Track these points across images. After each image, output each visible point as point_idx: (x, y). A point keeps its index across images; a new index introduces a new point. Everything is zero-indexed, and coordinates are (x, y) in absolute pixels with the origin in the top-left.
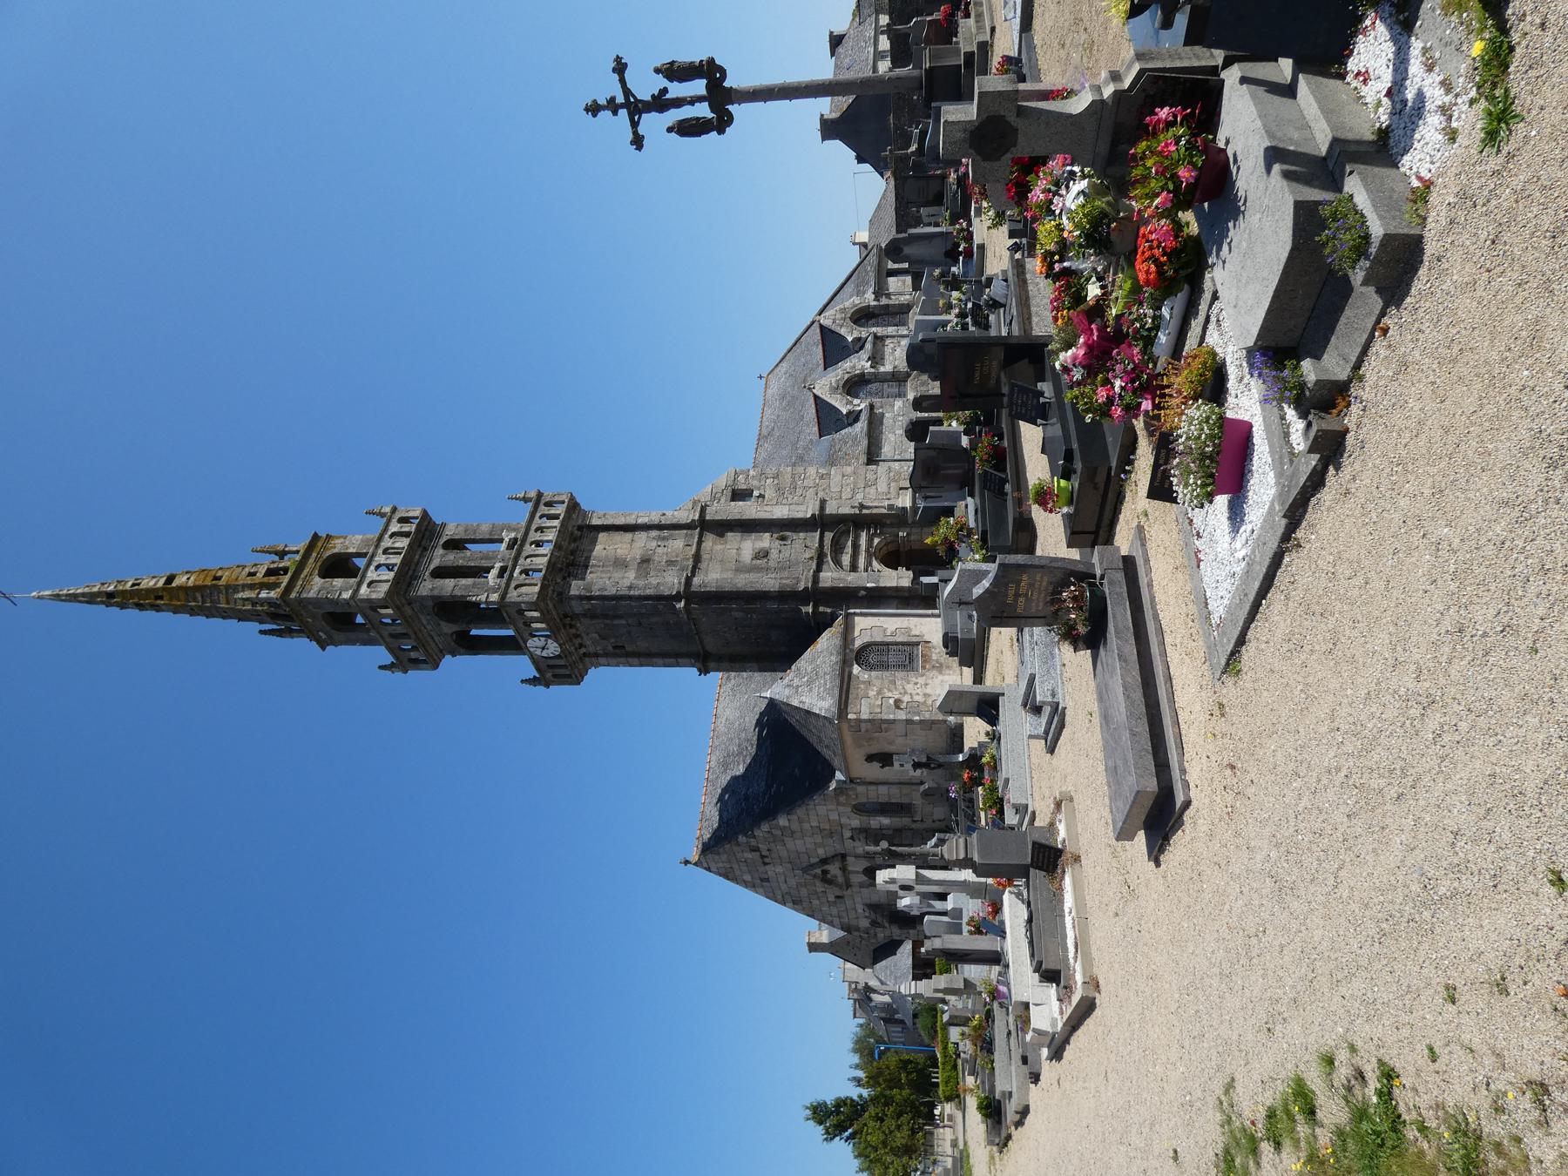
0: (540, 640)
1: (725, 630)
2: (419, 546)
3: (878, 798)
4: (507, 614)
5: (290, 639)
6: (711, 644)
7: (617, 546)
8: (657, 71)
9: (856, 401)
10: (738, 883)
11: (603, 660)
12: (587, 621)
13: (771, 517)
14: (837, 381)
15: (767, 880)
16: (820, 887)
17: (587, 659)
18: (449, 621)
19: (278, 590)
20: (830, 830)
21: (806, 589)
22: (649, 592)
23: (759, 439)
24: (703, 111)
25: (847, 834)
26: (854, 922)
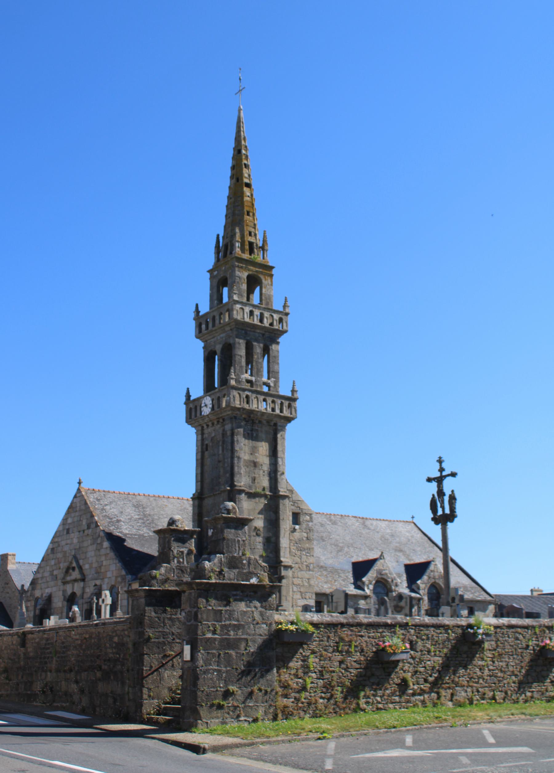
2: (266, 332)
5: (232, 155)
6: (208, 502)
7: (264, 447)
8: (453, 491)
9: (371, 587)
10: (66, 514)
11: (200, 437)
12: (221, 431)
14: (386, 574)
15: (68, 532)
16: (63, 565)
17: (200, 428)
19: (240, 253)
20: (101, 572)
22: (236, 469)
23: (363, 518)
24: (440, 512)
25: (98, 582)
26: (38, 587)
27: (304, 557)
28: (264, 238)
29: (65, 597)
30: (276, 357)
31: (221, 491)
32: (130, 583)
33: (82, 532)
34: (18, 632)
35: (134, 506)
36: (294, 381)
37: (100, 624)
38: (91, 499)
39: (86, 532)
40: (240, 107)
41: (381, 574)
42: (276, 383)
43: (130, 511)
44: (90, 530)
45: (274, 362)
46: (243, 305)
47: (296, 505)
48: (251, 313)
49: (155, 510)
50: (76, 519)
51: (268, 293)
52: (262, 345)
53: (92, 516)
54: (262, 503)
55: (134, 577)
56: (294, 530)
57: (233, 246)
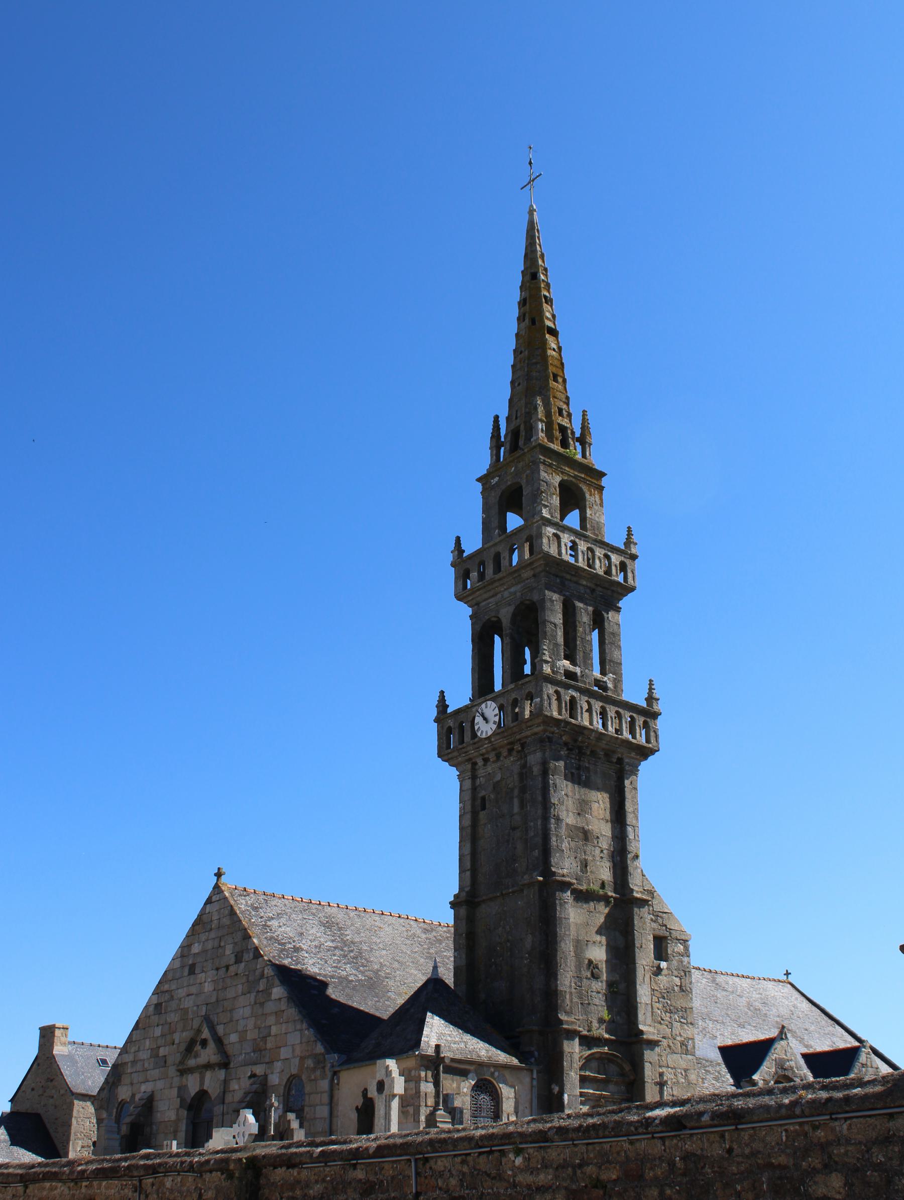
0: (495, 715)
1: (508, 927)
2: (597, 585)
3: (310, 1106)
4: (527, 682)
6: (488, 911)
7: (601, 802)
10: (187, 936)
11: (468, 784)
12: (516, 769)
13: (638, 982)
16: (181, 1037)
17: (469, 766)
18: (514, 615)
19: (546, 440)
21: (561, 1022)
25: (259, 1070)
26: (126, 1080)
27: (677, 1025)
28: (583, 424)
29: (182, 1100)
30: (616, 635)
31: (524, 885)
32: (336, 1069)
33: (224, 969)
34: (226, 1161)
35: (322, 924)
36: (651, 681)
37: (706, 1118)
38: (241, 905)
39: (232, 969)
40: (532, 206)
41: (782, 1068)
42: (617, 682)
43: (315, 931)
44: (242, 965)
45: (612, 643)
46: (558, 529)
47: (660, 920)
48: (574, 547)
49: (362, 935)
50: (209, 945)
51: (597, 519)
52: (590, 609)
53: (247, 937)
54: (602, 911)
55: (344, 1057)
56: (658, 971)
57: (530, 430)
